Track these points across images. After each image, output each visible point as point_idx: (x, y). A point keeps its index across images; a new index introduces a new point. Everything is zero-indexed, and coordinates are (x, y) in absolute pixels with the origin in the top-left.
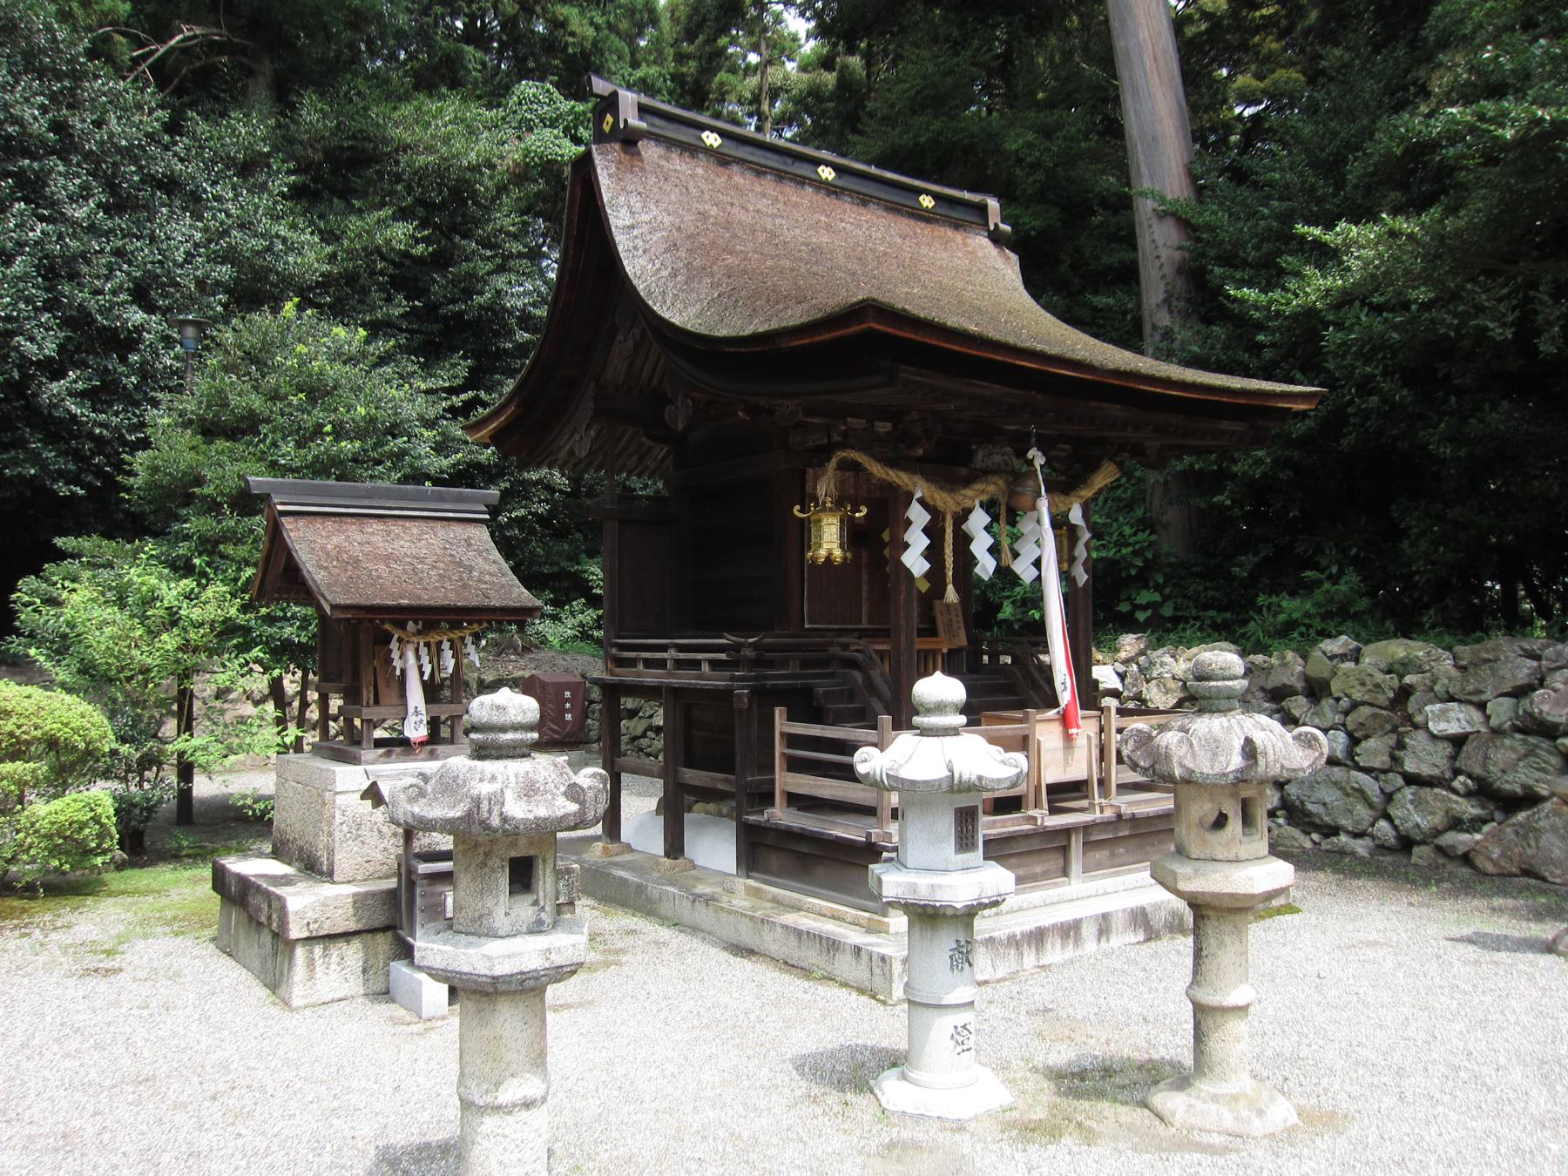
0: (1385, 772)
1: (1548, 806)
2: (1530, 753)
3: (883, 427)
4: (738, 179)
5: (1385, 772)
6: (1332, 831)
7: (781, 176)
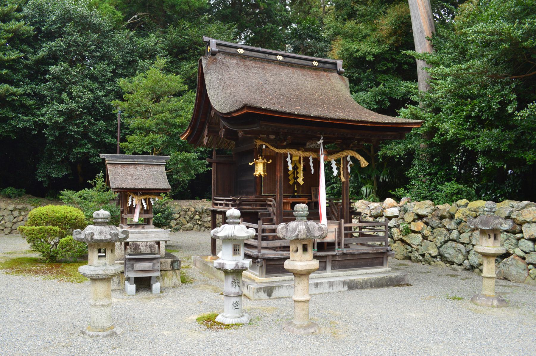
0: (468, 244)
1: (512, 257)
2: (508, 239)
3: (272, 137)
4: (248, 63)
5: (468, 244)
6: (452, 263)
7: (263, 60)
